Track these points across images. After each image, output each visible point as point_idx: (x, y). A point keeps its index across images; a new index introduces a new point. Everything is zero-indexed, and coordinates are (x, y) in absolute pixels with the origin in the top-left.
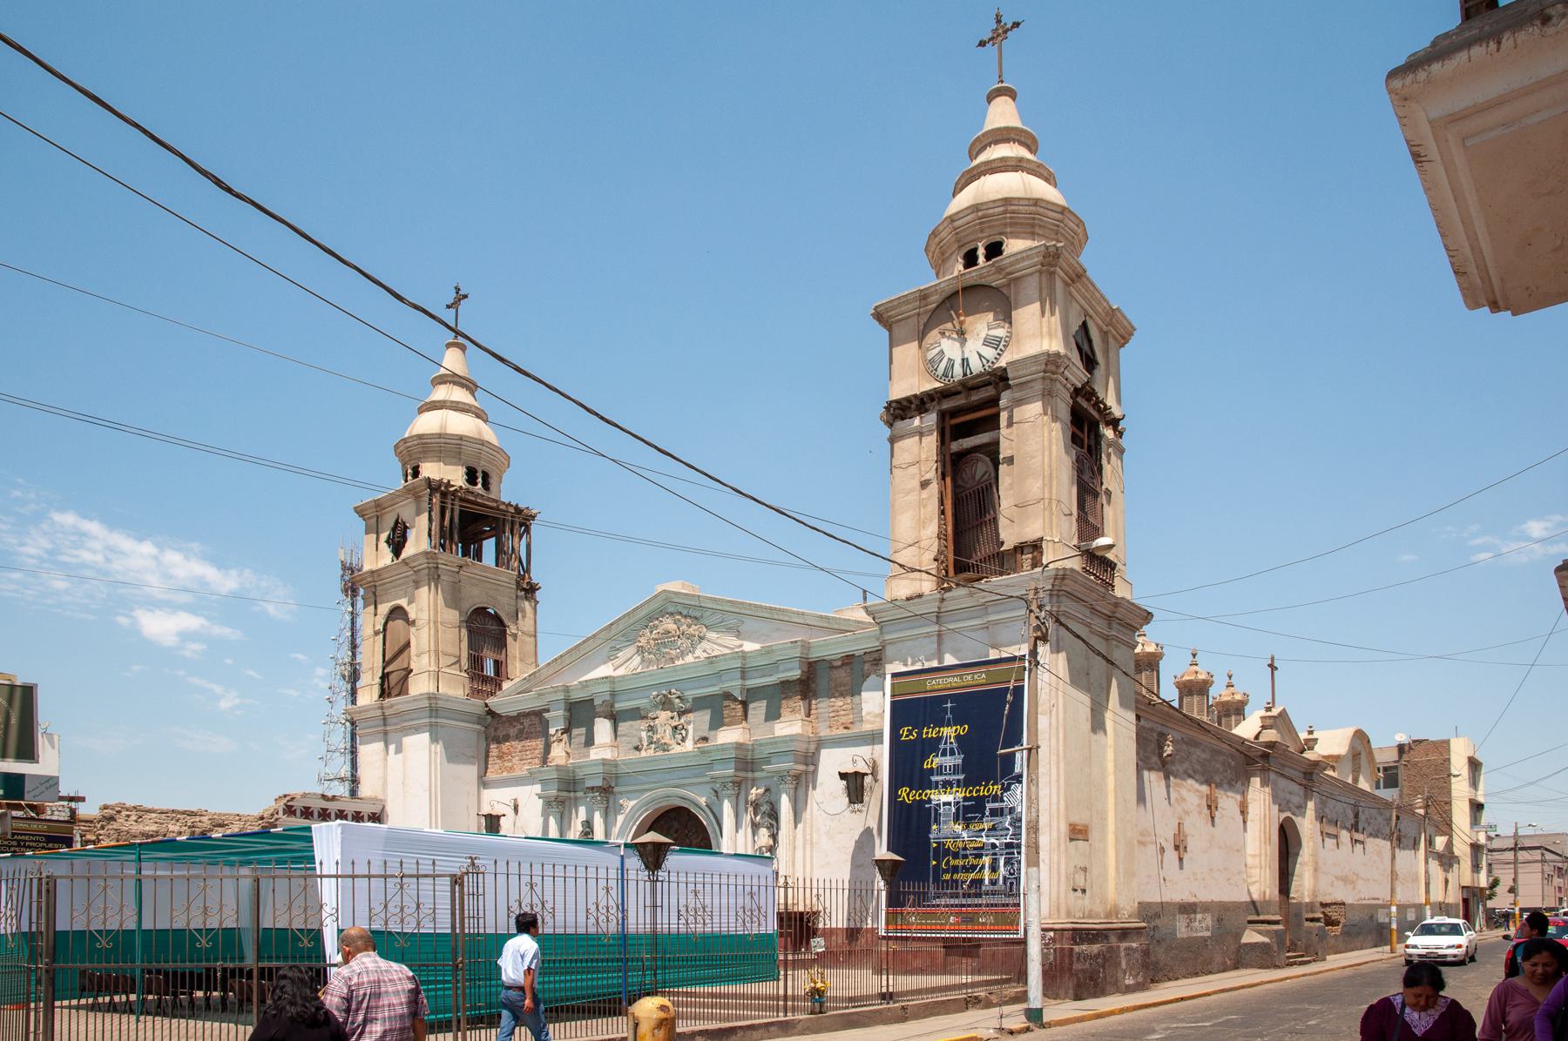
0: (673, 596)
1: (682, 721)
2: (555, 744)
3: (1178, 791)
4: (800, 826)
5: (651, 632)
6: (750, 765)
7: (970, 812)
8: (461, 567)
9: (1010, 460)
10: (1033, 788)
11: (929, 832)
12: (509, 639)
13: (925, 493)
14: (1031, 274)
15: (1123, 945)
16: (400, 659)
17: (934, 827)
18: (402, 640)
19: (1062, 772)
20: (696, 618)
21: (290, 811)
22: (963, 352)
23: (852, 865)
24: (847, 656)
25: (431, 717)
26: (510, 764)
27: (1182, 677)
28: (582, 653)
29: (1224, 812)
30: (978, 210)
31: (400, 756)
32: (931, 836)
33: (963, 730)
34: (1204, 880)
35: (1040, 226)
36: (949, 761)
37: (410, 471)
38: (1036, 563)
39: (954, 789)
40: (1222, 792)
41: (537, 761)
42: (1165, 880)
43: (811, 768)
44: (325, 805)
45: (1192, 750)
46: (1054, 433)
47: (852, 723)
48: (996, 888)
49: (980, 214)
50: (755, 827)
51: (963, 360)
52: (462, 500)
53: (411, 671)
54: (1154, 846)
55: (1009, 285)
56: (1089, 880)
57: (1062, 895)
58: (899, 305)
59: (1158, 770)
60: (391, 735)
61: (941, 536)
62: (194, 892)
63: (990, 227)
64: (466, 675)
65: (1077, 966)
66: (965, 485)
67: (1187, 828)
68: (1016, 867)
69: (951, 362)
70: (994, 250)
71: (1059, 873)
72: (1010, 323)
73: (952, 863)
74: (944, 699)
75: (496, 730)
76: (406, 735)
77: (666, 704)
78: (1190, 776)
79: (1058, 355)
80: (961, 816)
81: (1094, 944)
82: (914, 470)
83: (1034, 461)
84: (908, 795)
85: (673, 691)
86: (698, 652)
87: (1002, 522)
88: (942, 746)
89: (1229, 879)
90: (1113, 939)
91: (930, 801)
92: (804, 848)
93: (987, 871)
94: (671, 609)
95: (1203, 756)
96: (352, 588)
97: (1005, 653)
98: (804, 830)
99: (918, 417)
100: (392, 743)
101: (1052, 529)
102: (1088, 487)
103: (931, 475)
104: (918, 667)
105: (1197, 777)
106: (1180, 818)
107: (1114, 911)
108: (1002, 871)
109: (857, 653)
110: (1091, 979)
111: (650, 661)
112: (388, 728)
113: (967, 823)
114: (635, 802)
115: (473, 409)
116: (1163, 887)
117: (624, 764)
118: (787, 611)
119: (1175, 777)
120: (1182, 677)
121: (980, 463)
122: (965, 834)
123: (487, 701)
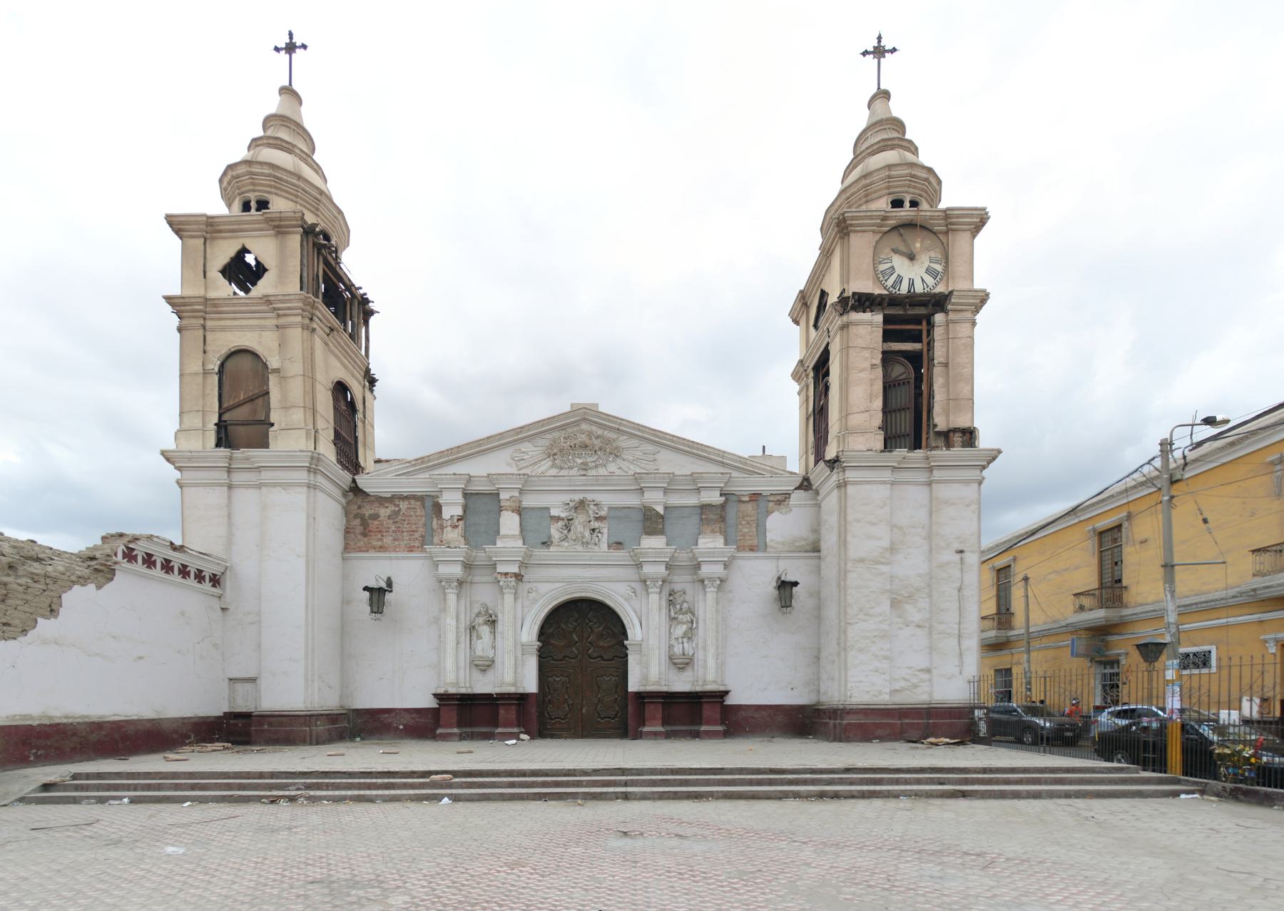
24: (754, 494)
44: (171, 554)
75: (359, 507)
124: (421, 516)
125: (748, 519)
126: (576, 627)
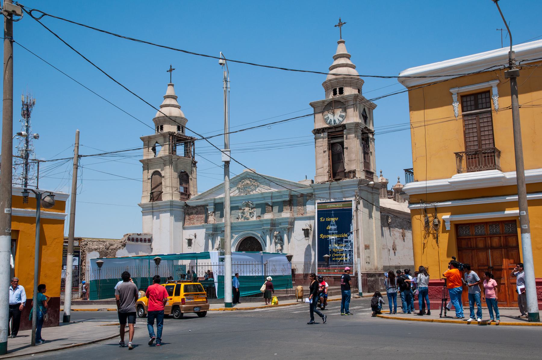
0: (249, 173)
1: (252, 211)
2: (210, 216)
3: (393, 232)
4: (289, 244)
5: (242, 183)
6: (274, 225)
7: (339, 241)
8: (178, 159)
9: (347, 148)
10: (358, 239)
11: (329, 246)
12: (190, 180)
13: (325, 154)
14: (351, 100)
15: (380, 278)
16: (158, 188)
17: (330, 245)
18: (158, 182)
19: (362, 231)
20: (256, 180)
21: (129, 239)
22: (334, 118)
23: (305, 255)
25: (170, 208)
26: (193, 222)
27: (395, 186)
28: (219, 188)
29: (407, 237)
30: (337, 79)
31: (158, 220)
32: (329, 248)
33: (337, 219)
34: (402, 259)
35: (352, 83)
36: (333, 227)
37: (159, 127)
38: (354, 176)
39: (335, 235)
40: (407, 231)
41: (203, 221)
42: (390, 259)
43: (293, 226)
45: (397, 219)
46: (358, 142)
47: (304, 213)
48: (347, 262)
49: (337, 80)
50: (276, 244)
51: (334, 120)
52: (177, 137)
53: (163, 192)
54: (387, 249)
55: (345, 102)
56: (370, 260)
57: (364, 264)
58: (317, 103)
59: (387, 227)
60: (155, 213)
61: (329, 166)
62: (253, 267)
63: (340, 84)
64: (179, 193)
65: (368, 284)
66: (334, 151)
67: (396, 243)
68: (352, 256)
69: (331, 120)
70: (341, 91)
71: (363, 258)
72: (346, 112)
73: (335, 255)
74: (331, 210)
75: (188, 211)
76: (161, 214)
77: (247, 205)
78: (396, 227)
79: (358, 123)
80: (337, 242)
81: (372, 277)
82: (321, 148)
83: (353, 149)
84: (323, 236)
85: (250, 202)
86: (257, 190)
87: (345, 164)
88: (331, 223)
89: (410, 258)
90: (377, 276)
91: (328, 238)
92: (291, 250)
93: (344, 258)
94: (248, 177)
95: (400, 221)
96: (27, 114)
97: (347, 199)
98: (291, 245)
99: (322, 134)
100: (155, 216)
101: (358, 167)
102: (366, 152)
103: (326, 149)
104: (324, 201)
105: (398, 227)
106: (394, 240)
107: (377, 269)
108: (348, 257)
109: (305, 194)
110: (372, 287)
111: (242, 192)
112: (154, 210)
113: (339, 244)
114: (238, 235)
115: (178, 106)
116: (390, 262)
117: (235, 223)
118: (284, 180)
119: (392, 228)
120: (395, 186)
121: (338, 146)
122: (338, 247)
123: (186, 202)
124: (204, 212)
125: (301, 203)
126: (249, 247)
